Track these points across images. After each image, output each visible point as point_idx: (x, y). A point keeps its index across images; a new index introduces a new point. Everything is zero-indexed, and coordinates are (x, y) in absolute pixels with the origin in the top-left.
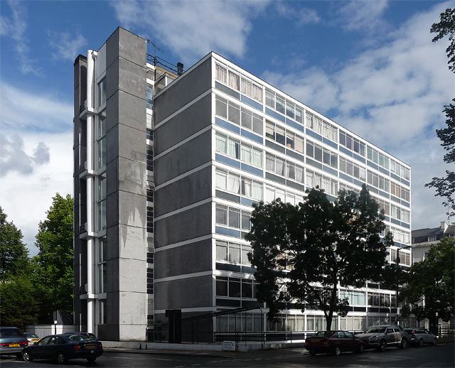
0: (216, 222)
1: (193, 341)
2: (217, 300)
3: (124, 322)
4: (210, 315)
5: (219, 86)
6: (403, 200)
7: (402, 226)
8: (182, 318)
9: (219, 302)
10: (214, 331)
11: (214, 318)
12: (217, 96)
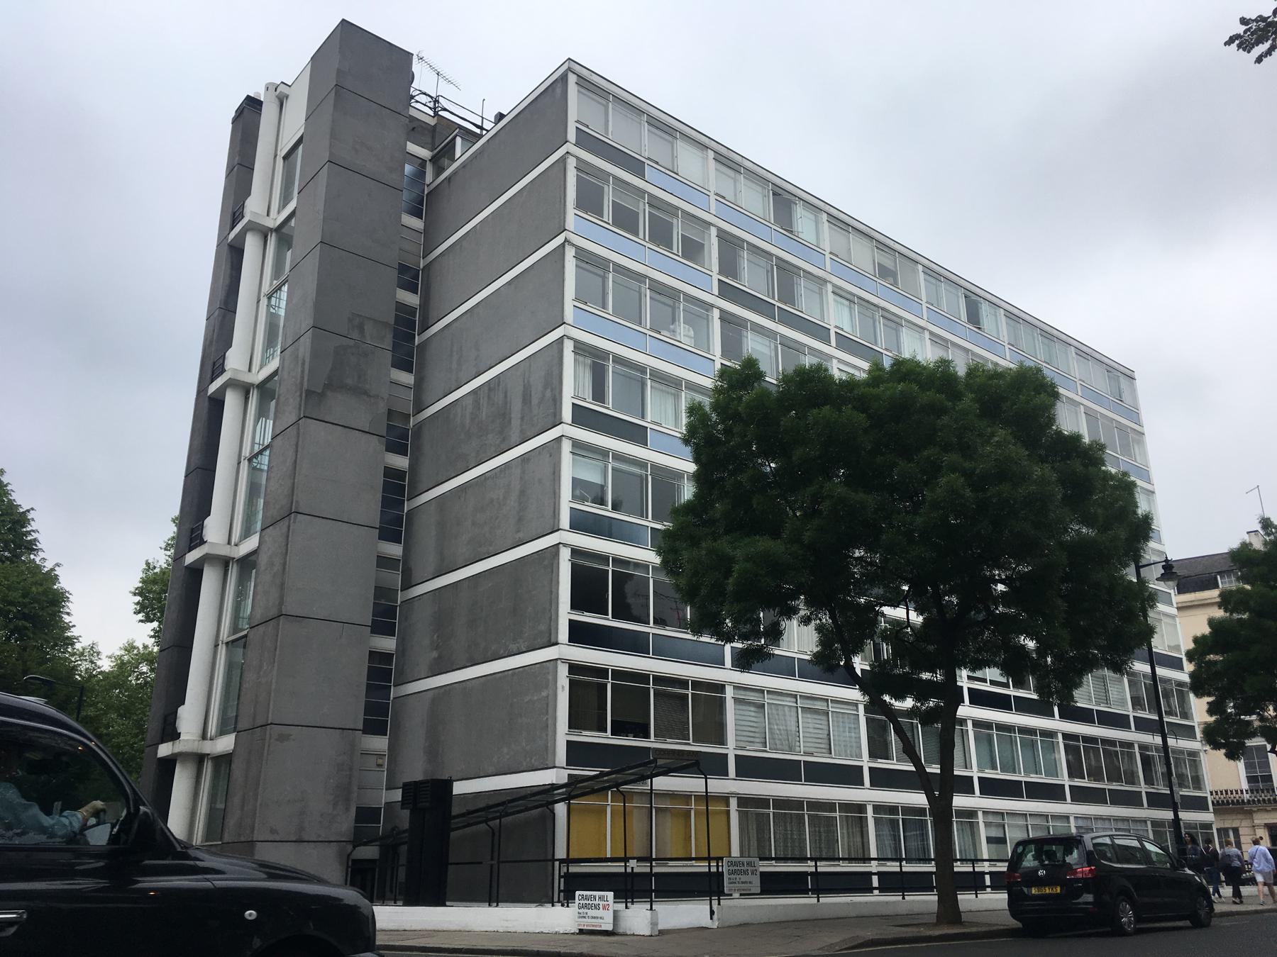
0: (572, 608)
1: (492, 897)
2: (572, 623)
3: (273, 831)
4: (546, 795)
5: (585, 140)
6: (1115, 786)
7: (1114, 803)
8: (456, 810)
9: (577, 753)
10: (561, 853)
11: (561, 809)
12: (582, 167)
